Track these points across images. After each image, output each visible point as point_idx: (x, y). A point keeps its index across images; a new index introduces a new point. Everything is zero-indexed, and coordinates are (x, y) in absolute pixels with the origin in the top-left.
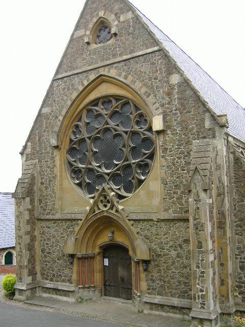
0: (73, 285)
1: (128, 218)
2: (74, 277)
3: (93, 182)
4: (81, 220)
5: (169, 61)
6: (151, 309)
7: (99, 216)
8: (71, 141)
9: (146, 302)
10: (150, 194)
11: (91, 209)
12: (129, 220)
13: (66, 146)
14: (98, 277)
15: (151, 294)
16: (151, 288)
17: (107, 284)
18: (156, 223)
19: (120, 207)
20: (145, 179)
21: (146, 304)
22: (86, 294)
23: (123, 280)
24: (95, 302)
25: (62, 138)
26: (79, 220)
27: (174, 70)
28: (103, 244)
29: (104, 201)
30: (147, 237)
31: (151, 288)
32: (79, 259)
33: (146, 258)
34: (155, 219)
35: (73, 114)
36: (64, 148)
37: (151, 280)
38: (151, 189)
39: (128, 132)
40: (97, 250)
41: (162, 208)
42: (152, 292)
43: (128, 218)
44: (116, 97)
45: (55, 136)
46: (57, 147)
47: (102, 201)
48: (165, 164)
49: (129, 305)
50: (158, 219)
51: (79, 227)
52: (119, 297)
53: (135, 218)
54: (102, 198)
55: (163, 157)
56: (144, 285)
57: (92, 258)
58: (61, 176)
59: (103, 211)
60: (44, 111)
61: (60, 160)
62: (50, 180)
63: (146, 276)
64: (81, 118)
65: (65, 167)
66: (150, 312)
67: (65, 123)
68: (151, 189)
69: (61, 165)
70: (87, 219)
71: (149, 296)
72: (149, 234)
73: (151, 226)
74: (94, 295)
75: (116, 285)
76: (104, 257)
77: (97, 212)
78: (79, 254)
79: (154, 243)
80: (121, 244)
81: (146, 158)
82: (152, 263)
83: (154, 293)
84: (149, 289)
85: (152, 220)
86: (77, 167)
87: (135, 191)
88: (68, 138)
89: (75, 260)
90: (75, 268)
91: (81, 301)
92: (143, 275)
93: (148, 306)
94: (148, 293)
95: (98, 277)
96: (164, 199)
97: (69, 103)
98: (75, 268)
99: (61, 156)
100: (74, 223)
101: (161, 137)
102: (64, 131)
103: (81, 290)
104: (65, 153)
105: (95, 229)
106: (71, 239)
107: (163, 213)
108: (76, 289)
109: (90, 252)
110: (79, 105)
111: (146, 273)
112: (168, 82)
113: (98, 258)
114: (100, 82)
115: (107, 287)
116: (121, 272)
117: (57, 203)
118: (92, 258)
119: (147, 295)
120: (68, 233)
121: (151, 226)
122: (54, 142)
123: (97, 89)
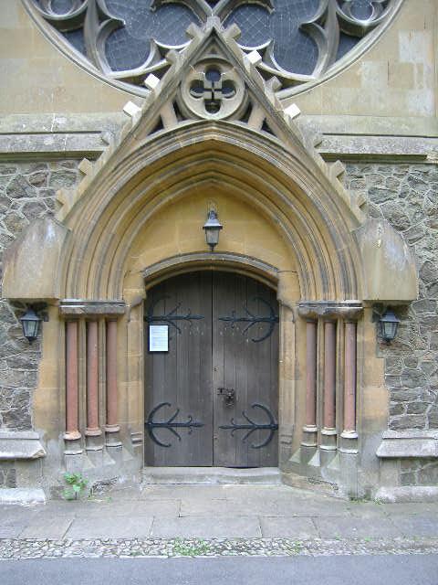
0: (36, 435)
1: (320, 150)
2: (43, 397)
3: (135, 24)
4: (93, 156)
6: (406, 480)
7: (182, 144)
9: (384, 459)
11: (145, 115)
12: (329, 158)
14: (132, 397)
15: (404, 428)
16: (405, 405)
17: (156, 420)
19: (290, 111)
20: (371, 28)
21: (388, 465)
22: (92, 464)
23: (230, 399)
24: (130, 489)
26: (79, 156)
28: (162, 266)
29: (207, 84)
30: (398, 225)
31: (405, 405)
32: (69, 320)
33: (401, 290)
37: (407, 375)
38: (404, 57)
39: (107, 18)
40: (135, 291)
42: (407, 419)
43: (320, 150)
47: (197, 87)
49: (267, 485)
51: (82, 186)
52: (213, 463)
53: (348, 147)
54: (199, 74)
56: (377, 397)
57: (110, 320)
59: (206, 123)
63: (389, 362)
66: (403, 491)
68: (404, 57)
70: (122, 157)
71: (396, 434)
72: (408, 212)
73: (414, 182)
74: (116, 463)
75: (197, 420)
76: (149, 320)
77: (172, 124)
78: (76, 301)
79: (424, 243)
80: (246, 261)
82: (413, 312)
83: (417, 420)
84: (394, 412)
87: (329, 63)
89: (52, 328)
90: (49, 360)
91: (69, 497)
92: (375, 364)
93: (392, 472)
94: (395, 426)
95: (130, 395)
98: (49, 360)
100: (50, 170)
103: (76, 450)
105: (142, 205)
106: (43, 233)
108: (55, 447)
109: (107, 296)
111: (387, 354)
113: (136, 321)
115: (160, 434)
116: (224, 370)
118: (110, 320)
119: (390, 433)
120: (19, 212)
121: (414, 182)
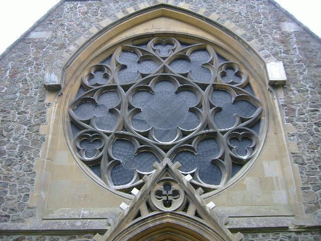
1: (228, 227)
4: (102, 232)
5: (276, 6)
7: (151, 225)
8: (83, 86)
10: (265, 183)
11: (131, 209)
12: (234, 231)
13: (72, 92)
18: (293, 235)
25: (68, 78)
27: (285, 18)
34: (291, 228)
35: (100, 47)
36: (67, 96)
41: (303, 206)
43: (228, 227)
44: (183, 40)
45: (60, 71)
46: (54, 89)
47: (159, 193)
48: (294, 130)
50: (301, 227)
53: (245, 225)
54: (160, 187)
55: (289, 121)
58: (54, 142)
59: (164, 213)
60: (33, 35)
61: (58, 113)
62: (24, 148)
64: (111, 56)
65: (63, 127)
67: (82, 56)
69: (56, 122)
77: (146, 214)
81: (247, 126)
85: (285, 229)
86: (92, 132)
88: (79, 79)
96: (304, 189)
97: (94, 30)
99: (59, 107)
101: (281, 93)
102: (74, 68)
104: (67, 107)
107: (306, 216)
110: (111, 38)
112: (280, 29)
114: (125, 28)
117: (34, 194)
122: (53, 79)
123: (153, 22)
